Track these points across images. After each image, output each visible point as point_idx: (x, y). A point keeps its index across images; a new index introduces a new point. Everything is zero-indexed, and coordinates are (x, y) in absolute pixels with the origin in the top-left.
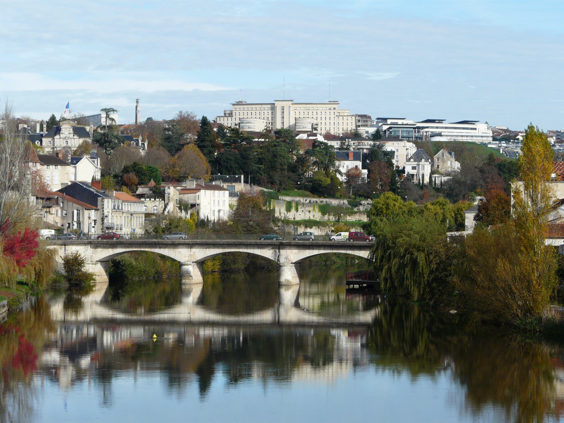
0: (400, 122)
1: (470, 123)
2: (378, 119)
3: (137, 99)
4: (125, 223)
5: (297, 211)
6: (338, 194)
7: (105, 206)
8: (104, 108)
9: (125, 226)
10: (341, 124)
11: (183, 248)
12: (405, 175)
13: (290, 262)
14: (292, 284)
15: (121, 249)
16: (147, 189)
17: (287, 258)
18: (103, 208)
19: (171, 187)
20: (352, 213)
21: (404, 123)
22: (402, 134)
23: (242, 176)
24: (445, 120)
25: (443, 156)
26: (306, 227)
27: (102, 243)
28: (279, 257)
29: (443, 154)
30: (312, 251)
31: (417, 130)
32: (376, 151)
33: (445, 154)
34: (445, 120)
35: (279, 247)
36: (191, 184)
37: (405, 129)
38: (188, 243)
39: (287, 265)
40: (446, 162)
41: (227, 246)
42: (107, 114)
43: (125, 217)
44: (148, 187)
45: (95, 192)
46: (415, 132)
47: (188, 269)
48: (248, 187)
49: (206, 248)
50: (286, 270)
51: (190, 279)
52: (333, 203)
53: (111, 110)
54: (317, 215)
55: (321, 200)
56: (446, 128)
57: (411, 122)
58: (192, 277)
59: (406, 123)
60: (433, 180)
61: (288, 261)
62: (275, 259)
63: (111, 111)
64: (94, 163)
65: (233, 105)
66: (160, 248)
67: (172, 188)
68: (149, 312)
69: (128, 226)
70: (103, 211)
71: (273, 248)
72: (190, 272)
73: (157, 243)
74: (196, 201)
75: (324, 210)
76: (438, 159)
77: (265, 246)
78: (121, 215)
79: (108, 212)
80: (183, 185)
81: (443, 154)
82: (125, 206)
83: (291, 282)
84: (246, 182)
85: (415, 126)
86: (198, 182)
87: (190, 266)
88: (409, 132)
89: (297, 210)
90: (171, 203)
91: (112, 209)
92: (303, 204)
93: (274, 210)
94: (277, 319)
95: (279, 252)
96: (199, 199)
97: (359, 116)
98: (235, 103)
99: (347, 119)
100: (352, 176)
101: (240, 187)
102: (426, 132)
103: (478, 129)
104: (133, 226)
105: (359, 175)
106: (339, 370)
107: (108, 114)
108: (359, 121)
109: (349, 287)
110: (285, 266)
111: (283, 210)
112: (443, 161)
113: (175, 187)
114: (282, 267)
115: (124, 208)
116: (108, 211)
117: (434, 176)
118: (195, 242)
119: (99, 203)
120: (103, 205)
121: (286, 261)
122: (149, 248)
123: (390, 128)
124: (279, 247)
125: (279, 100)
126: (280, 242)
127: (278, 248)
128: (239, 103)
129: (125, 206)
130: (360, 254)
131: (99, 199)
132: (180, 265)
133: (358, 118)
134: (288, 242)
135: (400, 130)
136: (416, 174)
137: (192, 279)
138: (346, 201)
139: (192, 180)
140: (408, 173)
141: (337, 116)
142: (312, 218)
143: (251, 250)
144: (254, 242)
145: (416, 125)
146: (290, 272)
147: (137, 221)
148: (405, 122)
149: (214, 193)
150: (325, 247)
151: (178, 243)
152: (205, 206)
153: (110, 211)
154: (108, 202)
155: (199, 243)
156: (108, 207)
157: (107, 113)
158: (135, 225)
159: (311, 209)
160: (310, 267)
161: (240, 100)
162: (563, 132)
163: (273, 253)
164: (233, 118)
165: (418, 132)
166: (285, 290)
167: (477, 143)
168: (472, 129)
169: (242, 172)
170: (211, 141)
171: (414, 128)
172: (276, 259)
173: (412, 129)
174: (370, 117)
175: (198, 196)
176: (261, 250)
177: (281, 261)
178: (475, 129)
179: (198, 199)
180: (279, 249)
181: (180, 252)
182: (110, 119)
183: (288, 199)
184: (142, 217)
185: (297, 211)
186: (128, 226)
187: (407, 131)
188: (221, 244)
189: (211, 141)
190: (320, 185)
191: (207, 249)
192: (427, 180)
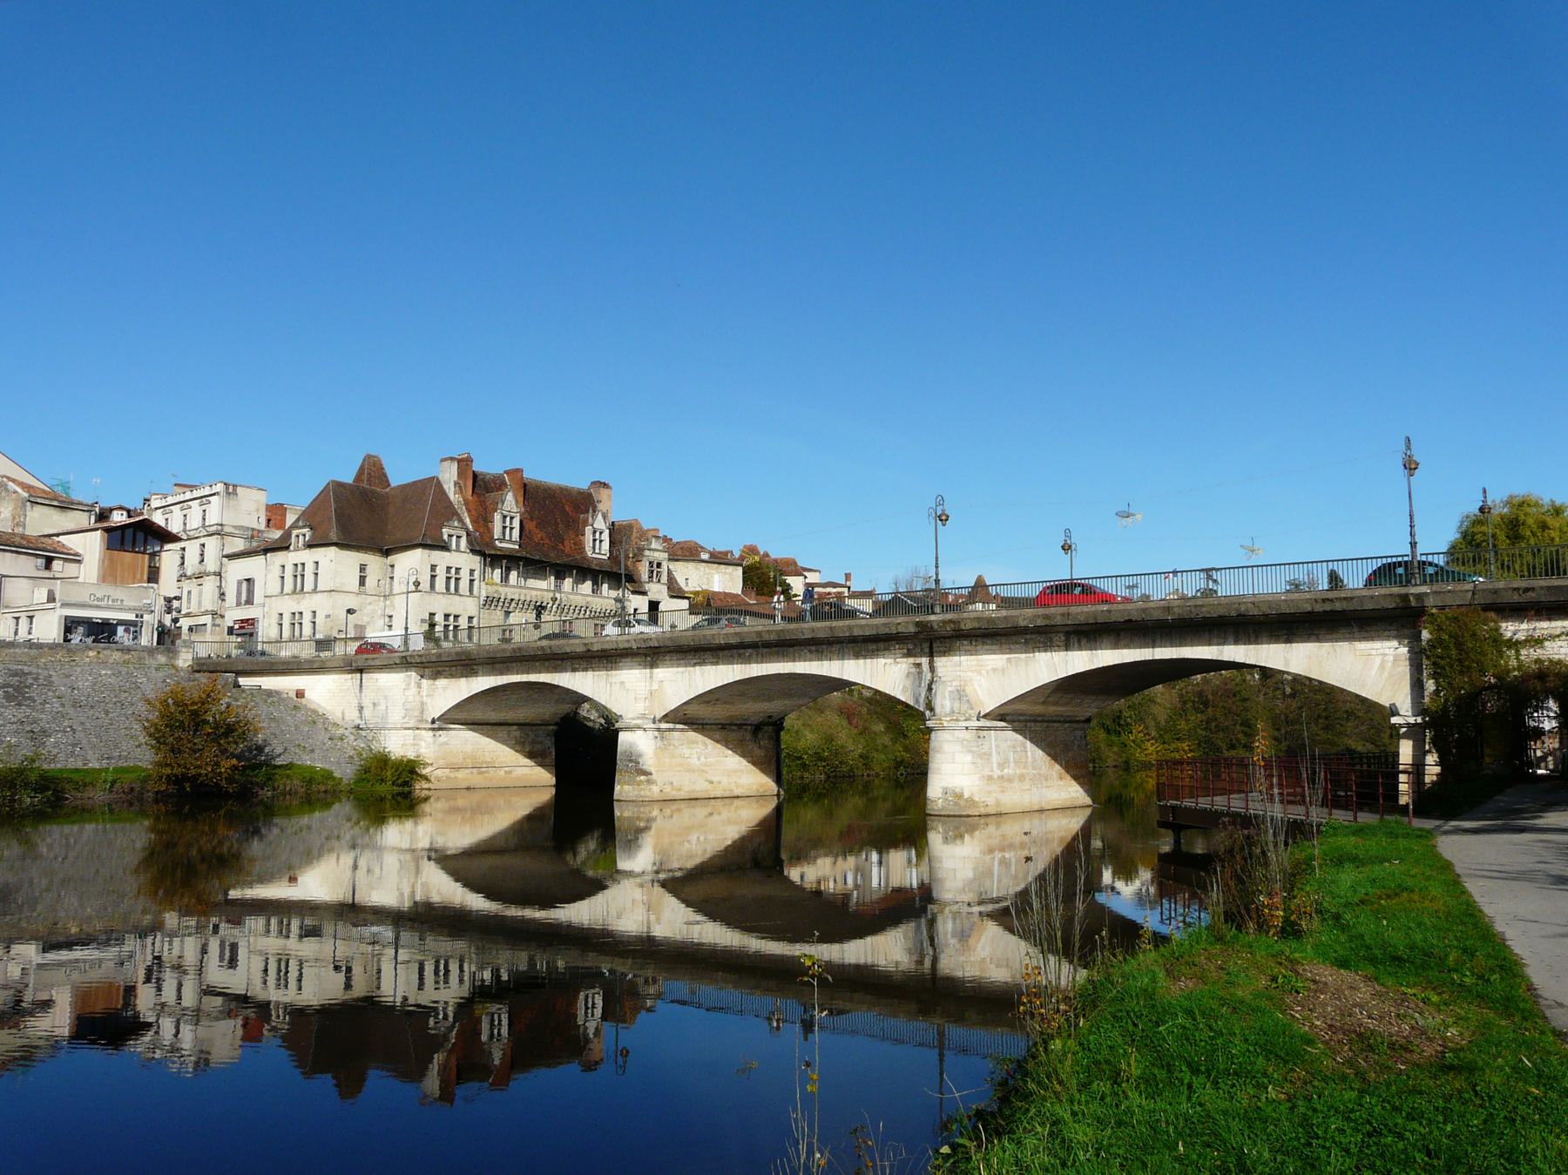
11: (994, 653)
13: (974, 713)
14: (983, 811)
15: (722, 668)
17: (960, 695)
28: (930, 689)
30: (1062, 654)
35: (931, 648)
39: (952, 724)
49: (695, 665)
50: (947, 747)
51: (639, 783)
61: (965, 707)
62: (917, 701)
71: (909, 654)
83: (971, 802)
87: (640, 733)
94: (927, 963)
95: (932, 669)
109: (1177, 842)
110: (943, 729)
114: (933, 735)
121: (956, 705)
122: (548, 670)
124: (931, 648)
126: (917, 624)
127: (927, 650)
130: (1287, 662)
134: (951, 621)
144: (823, 629)
146: (969, 758)
162: (1565, 1033)
163: (908, 675)
166: (946, 840)
172: (922, 700)
176: (868, 661)
180: (931, 655)
181: (622, 683)
191: (697, 668)
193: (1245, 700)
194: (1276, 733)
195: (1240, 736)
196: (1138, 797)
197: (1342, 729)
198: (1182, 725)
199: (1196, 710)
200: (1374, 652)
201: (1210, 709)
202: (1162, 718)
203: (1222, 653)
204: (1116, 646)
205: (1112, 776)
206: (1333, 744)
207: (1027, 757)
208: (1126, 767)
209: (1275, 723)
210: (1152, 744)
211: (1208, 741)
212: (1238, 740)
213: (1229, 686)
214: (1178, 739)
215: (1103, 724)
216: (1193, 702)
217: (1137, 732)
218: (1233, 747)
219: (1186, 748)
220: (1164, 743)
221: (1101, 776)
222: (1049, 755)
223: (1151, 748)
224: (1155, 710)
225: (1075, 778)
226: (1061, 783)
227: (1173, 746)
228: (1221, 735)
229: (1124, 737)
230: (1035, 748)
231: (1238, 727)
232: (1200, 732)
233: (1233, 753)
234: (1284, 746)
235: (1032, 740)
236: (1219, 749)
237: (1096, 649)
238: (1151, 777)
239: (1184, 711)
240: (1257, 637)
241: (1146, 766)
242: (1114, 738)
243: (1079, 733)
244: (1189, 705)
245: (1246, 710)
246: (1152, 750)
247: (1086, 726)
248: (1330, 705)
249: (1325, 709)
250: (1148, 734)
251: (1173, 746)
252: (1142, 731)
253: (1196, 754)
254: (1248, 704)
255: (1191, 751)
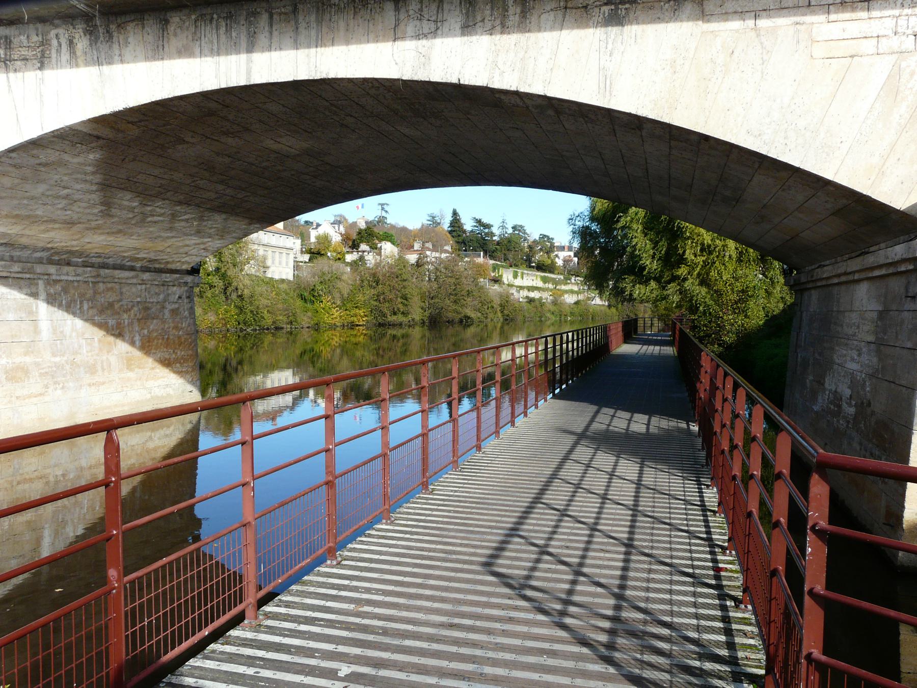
6: (556, 272)
20: (566, 284)
26: (529, 290)
54: (540, 284)
69: (280, 263)
75: (545, 280)
89: (522, 278)
93: (501, 276)
100: (567, 261)
105: (571, 261)
106: (58, 57)
111: (511, 277)
138: (562, 277)
142: (535, 285)
149: (248, 78)
159: (534, 278)
160: (524, 322)
190: (543, 265)
193: (405, 280)
194: (423, 304)
195: (400, 306)
196: (326, 352)
197: (465, 302)
198: (360, 297)
199: (371, 286)
200: (868, 46)
201: (380, 286)
202: (345, 293)
203: (426, 58)
204: (157, 52)
205: (305, 336)
206: (458, 313)
207: (37, 331)
208: (316, 328)
209: (422, 298)
210: (337, 311)
211: (377, 309)
212: (398, 309)
213: (395, 270)
214: (356, 307)
215: (301, 295)
216: (369, 281)
217: (326, 301)
218: (395, 314)
219: (362, 314)
220: (346, 310)
221: (296, 335)
222: (101, 326)
223: (336, 313)
224: (340, 285)
225: (167, 363)
226: (130, 375)
227: (353, 312)
228: (387, 305)
229: (317, 305)
230: (60, 315)
231: (399, 300)
232: (373, 302)
233: (394, 318)
234: (427, 314)
235: (51, 300)
236: (384, 315)
237: (110, 62)
238: (335, 335)
239: (362, 287)
240: (524, 14)
241: (333, 327)
242: (309, 305)
243: (177, 291)
244: (366, 283)
245: (404, 287)
246: (336, 315)
247: (189, 279)
248: (458, 287)
249: (455, 290)
250: (334, 303)
251: (353, 312)
252: (330, 300)
253: (369, 319)
254: (405, 283)
255: (366, 316)
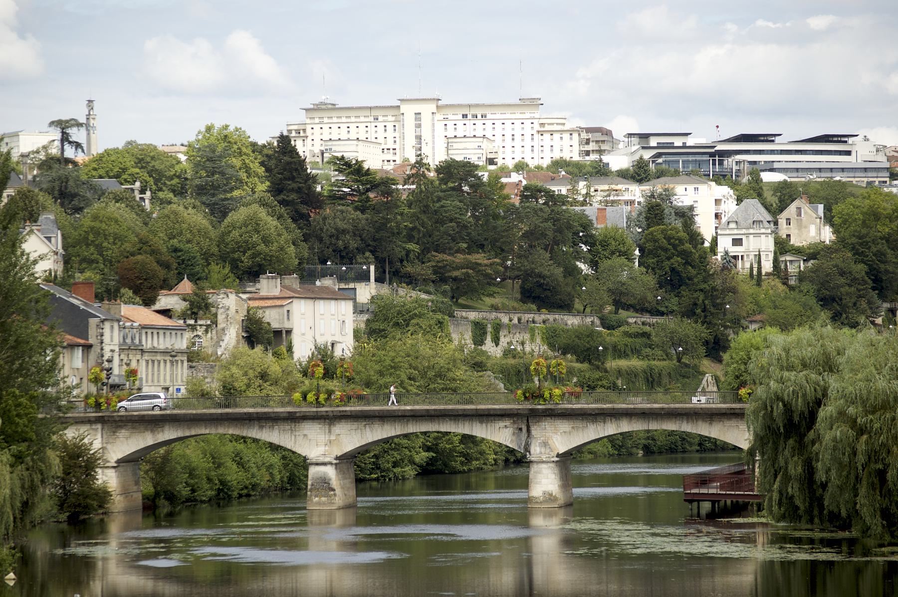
0: (678, 142)
1: (835, 139)
2: (630, 135)
3: (89, 101)
4: (147, 375)
5: (497, 345)
7: (107, 338)
8: (56, 119)
9: (147, 381)
10: (547, 148)
12: (719, 257)
16: (176, 298)
18: (102, 343)
19: (230, 295)
21: (687, 145)
22: (684, 167)
23: (372, 268)
24: (780, 135)
25: (799, 214)
27: (129, 418)
29: (799, 209)
31: (717, 158)
32: (658, 205)
33: (805, 210)
34: (780, 135)
36: (268, 286)
37: (691, 158)
38: (324, 414)
40: (806, 227)
41: (410, 418)
42: (63, 133)
43: (147, 362)
44: (178, 294)
45: (82, 307)
46: (714, 164)
47: (325, 473)
48: (385, 290)
52: (569, 322)
53: (73, 122)
55: (543, 317)
56: (783, 152)
57: (702, 141)
58: (333, 490)
59: (692, 144)
60: (783, 266)
63: (73, 126)
64: (50, 241)
65: (307, 110)
66: (261, 427)
67: (233, 297)
68: (771, 543)
69: (153, 381)
70: (102, 349)
72: (330, 480)
73: (255, 415)
74: (283, 323)
76: (788, 221)
77: (497, 418)
78: (139, 357)
79: (112, 351)
80: (248, 289)
81: (799, 209)
82: (147, 337)
84: (379, 280)
85: (713, 150)
86: (286, 281)
88: (699, 163)
90: (232, 328)
91: (120, 345)
92: (508, 326)
95: (529, 431)
96: (290, 318)
97: (589, 130)
98: (312, 106)
99: (561, 138)
101: (365, 292)
102: (738, 163)
103: (854, 154)
104: (165, 381)
107: (66, 133)
108: (588, 142)
112: (800, 226)
113: (237, 293)
115: (144, 343)
116: (112, 347)
117: (783, 259)
118: (340, 411)
119: (92, 332)
120: (102, 335)
123: (659, 155)
125: (408, 97)
128: (319, 108)
129: (147, 337)
131: (93, 322)
132: (304, 464)
133: (584, 136)
135: (681, 159)
136: (742, 256)
137: (335, 495)
139: (272, 278)
140: (726, 253)
141: (538, 132)
143: (448, 426)
145: (716, 149)
147: (159, 371)
148: (690, 141)
150: (631, 417)
151: (302, 414)
152: (304, 334)
153: (117, 349)
154: (112, 327)
155: (349, 414)
156: (112, 341)
157: (63, 129)
158: (168, 378)
161: (322, 98)
164: (309, 141)
165: (721, 163)
167: (854, 182)
168: (840, 153)
169: (372, 258)
170: (299, 191)
171: (712, 155)
173: (706, 158)
174: (608, 133)
175: (288, 311)
177: (532, 451)
178: (848, 153)
179: (288, 318)
182: (70, 142)
183: (473, 315)
184: (182, 361)
185: (497, 345)
186: (153, 381)
187: (696, 161)
188: (399, 416)
189: (299, 191)
192: (767, 266)
